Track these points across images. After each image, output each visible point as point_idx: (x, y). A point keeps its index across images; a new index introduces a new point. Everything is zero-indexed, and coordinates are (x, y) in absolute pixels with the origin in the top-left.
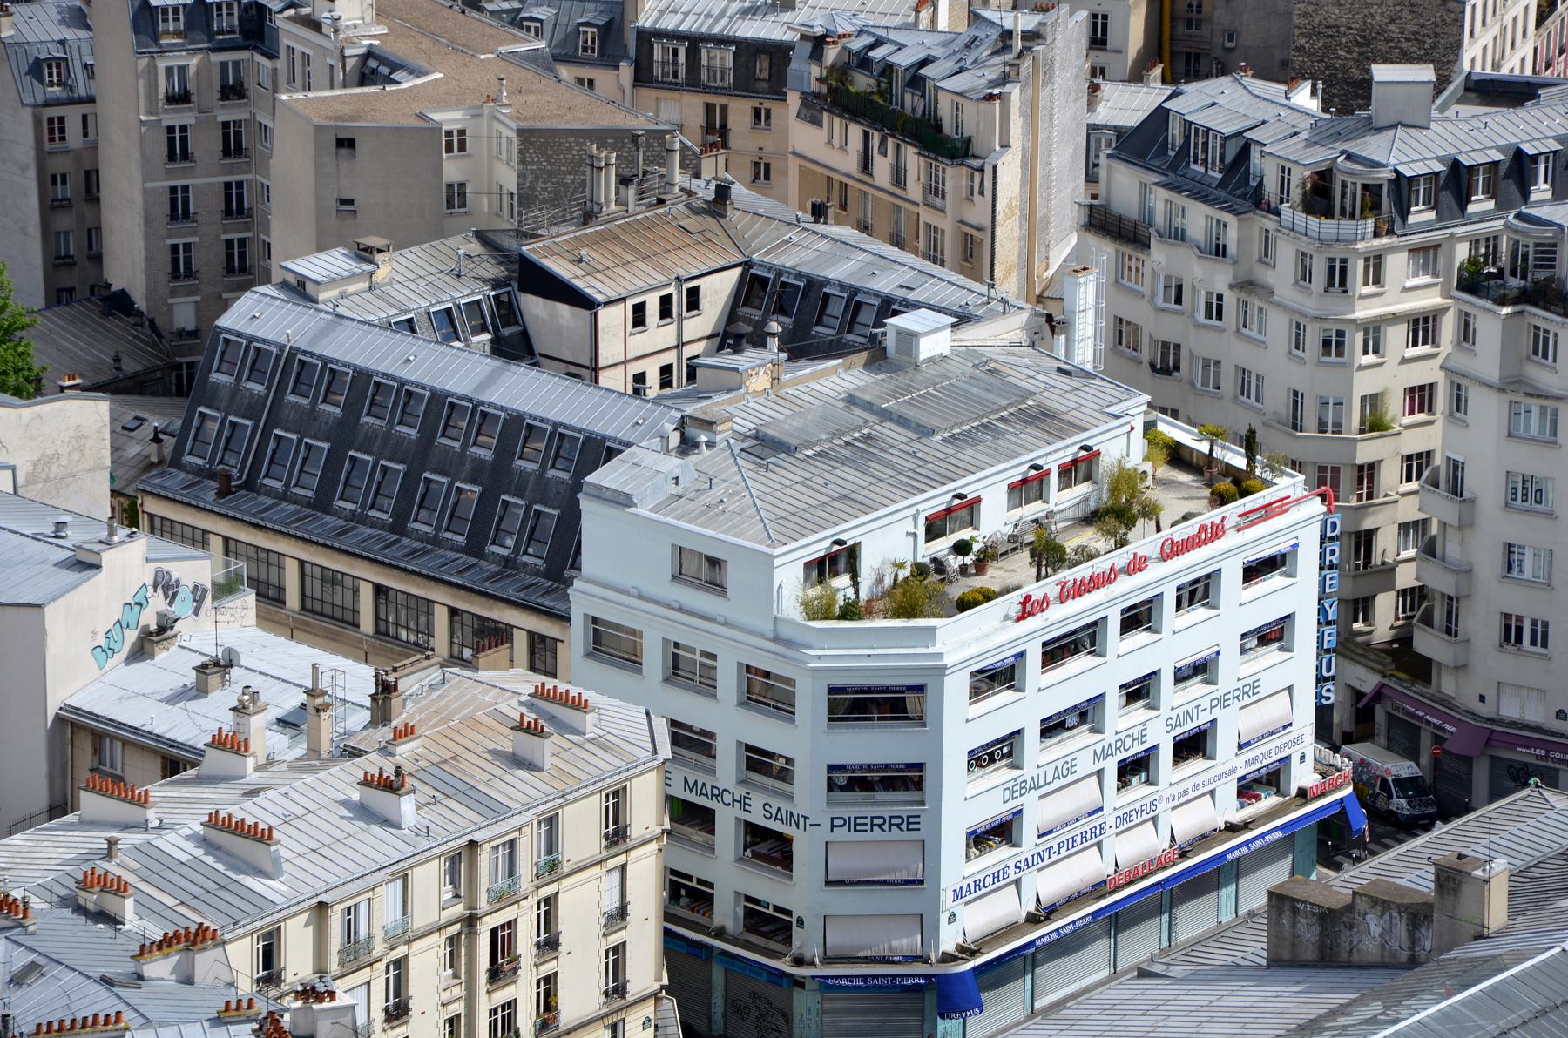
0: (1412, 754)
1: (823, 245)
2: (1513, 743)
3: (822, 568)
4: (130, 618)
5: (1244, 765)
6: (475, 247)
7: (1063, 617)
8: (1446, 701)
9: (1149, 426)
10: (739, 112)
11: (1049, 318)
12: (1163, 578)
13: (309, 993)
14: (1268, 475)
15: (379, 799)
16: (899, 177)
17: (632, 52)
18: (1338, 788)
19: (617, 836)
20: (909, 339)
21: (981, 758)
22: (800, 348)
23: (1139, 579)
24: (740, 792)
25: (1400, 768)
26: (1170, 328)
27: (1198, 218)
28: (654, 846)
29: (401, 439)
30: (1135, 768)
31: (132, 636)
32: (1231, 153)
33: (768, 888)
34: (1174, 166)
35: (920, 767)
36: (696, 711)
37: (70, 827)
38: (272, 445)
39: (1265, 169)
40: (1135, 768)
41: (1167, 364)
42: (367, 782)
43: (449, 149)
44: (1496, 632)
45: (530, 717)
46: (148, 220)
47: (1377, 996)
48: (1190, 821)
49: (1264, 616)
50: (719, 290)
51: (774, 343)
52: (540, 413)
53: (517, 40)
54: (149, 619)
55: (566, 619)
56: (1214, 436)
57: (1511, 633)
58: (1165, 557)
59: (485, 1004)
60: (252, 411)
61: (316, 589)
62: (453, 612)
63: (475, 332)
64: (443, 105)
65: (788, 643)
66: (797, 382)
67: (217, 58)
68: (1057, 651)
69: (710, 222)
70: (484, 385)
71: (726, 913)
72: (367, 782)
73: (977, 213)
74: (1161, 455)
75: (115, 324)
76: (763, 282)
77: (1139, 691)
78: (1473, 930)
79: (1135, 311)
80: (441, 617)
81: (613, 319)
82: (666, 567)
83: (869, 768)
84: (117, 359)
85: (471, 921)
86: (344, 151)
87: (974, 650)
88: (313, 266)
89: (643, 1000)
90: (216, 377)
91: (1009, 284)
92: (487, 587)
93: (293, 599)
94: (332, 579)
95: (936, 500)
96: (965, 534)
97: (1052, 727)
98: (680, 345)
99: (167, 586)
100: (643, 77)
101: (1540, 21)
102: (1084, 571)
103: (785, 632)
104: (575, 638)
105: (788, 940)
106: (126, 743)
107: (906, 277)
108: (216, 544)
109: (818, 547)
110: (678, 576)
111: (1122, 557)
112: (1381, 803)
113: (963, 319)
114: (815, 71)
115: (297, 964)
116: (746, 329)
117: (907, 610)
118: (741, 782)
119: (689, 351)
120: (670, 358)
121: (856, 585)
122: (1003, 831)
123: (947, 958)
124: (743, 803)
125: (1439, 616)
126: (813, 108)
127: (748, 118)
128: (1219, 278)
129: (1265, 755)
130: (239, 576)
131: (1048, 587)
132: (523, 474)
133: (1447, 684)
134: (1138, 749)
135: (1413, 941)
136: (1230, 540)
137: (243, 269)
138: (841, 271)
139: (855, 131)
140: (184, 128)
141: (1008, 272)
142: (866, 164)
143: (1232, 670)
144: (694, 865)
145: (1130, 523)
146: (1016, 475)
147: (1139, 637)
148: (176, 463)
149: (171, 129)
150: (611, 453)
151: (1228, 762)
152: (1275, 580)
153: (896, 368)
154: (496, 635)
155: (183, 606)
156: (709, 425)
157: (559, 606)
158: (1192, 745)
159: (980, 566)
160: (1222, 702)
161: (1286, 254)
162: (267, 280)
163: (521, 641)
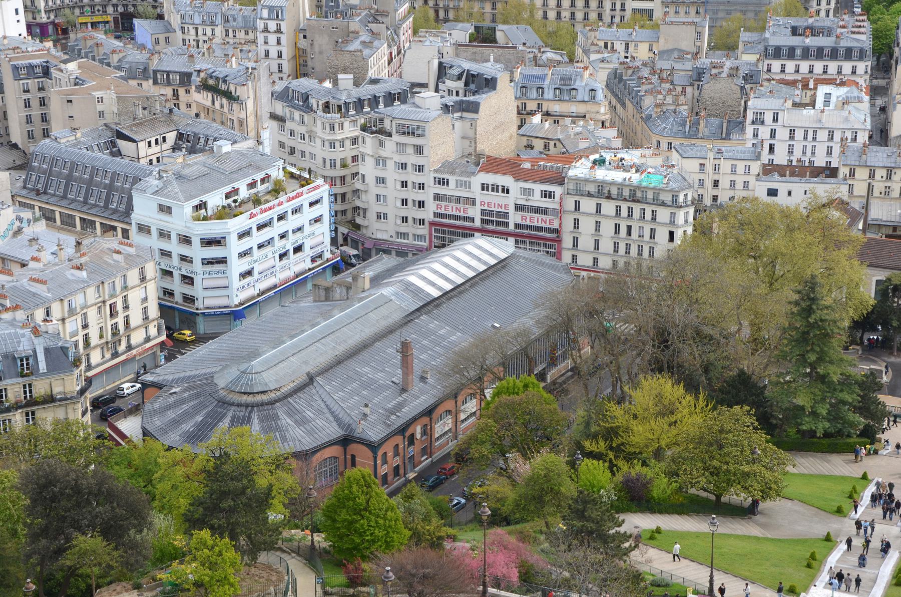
0: (357, 249)
3: (198, 207)
4: (10, 228)
5: (312, 253)
7: (262, 218)
8: (364, 235)
9: (284, 169)
10: (182, 92)
12: (288, 207)
14: (314, 179)
16: (222, 106)
17: (152, 76)
21: (242, 255)
23: (281, 207)
25: (354, 252)
27: (297, 114)
30: (282, 256)
31: (11, 233)
32: (305, 98)
33: (188, 290)
34: (290, 101)
35: (226, 258)
36: (166, 246)
39: (313, 102)
40: (282, 256)
43: (98, 102)
46: (20, 124)
48: (298, 268)
49: (316, 215)
50: (171, 137)
51: (184, 150)
53: (117, 73)
54: (15, 228)
56: (301, 169)
57: (379, 216)
58: (288, 201)
59: (110, 323)
60: (44, 173)
64: (95, 90)
66: (190, 160)
67: (36, 80)
68: (260, 227)
71: (178, 298)
73: (242, 115)
74: (288, 176)
75: (14, 152)
77: (283, 236)
78: (361, 290)
79: (283, 139)
80: (98, 225)
83: (212, 259)
85: (104, 302)
86: (69, 104)
87: (238, 227)
89: (92, 306)
90: (34, 164)
92: (110, 217)
94: (70, 216)
95: (228, 189)
96: (235, 198)
97: (260, 246)
99: (20, 220)
100: (155, 82)
101: (389, 64)
102: (267, 206)
105: (194, 304)
109: (196, 202)
111: (277, 201)
112: (349, 261)
113: (234, 143)
114: (198, 79)
117: (220, 217)
121: (206, 212)
122: (249, 273)
123: (236, 306)
126: (199, 89)
127: (185, 92)
128: (302, 130)
129: (318, 250)
131: (257, 210)
132: (117, 186)
134: (284, 251)
135: (347, 294)
136: (305, 196)
139: (210, 95)
140: (28, 99)
141: (252, 130)
142: (213, 103)
143: (307, 229)
145: (278, 193)
147: (282, 222)
149: (25, 100)
151: (308, 252)
152: (318, 206)
155: (25, 224)
157: (129, 222)
158: (298, 249)
159: (240, 205)
160: (305, 238)
161: (319, 123)
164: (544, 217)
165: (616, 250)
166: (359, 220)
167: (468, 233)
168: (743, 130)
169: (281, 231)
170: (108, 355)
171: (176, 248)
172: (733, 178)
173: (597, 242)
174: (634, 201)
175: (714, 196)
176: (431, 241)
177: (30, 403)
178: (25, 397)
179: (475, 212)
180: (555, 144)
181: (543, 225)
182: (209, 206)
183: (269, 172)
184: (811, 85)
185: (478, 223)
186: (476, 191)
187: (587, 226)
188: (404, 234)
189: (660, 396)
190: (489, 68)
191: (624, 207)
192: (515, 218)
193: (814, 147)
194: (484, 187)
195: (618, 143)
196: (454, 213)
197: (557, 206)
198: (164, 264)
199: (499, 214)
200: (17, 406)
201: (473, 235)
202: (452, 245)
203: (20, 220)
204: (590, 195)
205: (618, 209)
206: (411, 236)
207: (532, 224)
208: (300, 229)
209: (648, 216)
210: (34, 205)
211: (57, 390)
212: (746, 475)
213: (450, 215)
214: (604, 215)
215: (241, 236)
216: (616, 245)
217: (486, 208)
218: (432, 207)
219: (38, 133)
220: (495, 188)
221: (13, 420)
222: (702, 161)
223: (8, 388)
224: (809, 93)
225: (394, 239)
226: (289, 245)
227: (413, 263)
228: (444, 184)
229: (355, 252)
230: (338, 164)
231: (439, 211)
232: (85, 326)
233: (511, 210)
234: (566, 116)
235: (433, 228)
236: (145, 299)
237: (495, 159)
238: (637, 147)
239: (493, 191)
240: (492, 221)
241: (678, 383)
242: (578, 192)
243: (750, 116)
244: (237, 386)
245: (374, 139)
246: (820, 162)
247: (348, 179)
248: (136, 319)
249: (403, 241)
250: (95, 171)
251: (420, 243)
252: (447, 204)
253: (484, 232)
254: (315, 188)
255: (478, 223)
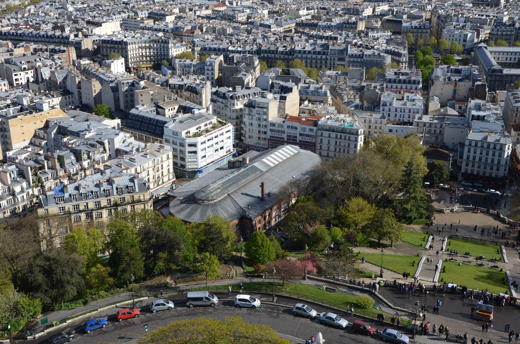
3: (187, 133)
7: (209, 137)
12: (219, 133)
16: (194, 96)
21: (202, 150)
33: (183, 163)
50: (177, 107)
94: (141, 135)
95: (197, 126)
99: (125, 137)
109: (186, 131)
122: (205, 156)
151: (225, 149)
158: (222, 148)
168: (379, 108)
170: (156, 185)
172: (376, 125)
173: (329, 147)
174: (342, 133)
177: (133, 202)
179: (285, 136)
182: (191, 132)
183: (212, 120)
184: (402, 93)
185: (286, 139)
187: (325, 141)
189: (358, 205)
190: (290, 84)
192: (299, 138)
193: (404, 115)
194: (288, 127)
195: (336, 112)
199: (293, 137)
200: (129, 203)
208: (222, 141)
211: (142, 198)
212: (390, 233)
215: (202, 143)
216: (336, 148)
218: (269, 134)
224: (401, 96)
226: (218, 147)
227: (264, 154)
229: (241, 149)
232: (148, 175)
236: (169, 166)
237: (292, 117)
238: (342, 113)
241: (365, 200)
243: (381, 103)
246: (406, 120)
248: (165, 173)
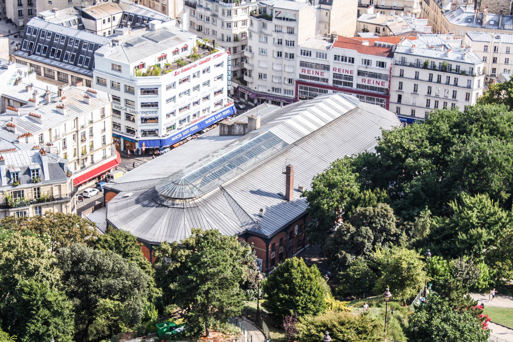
1: (137, 8)
2: (261, 96)
6: (73, 9)
7: (183, 76)
8: (249, 89)
9: (197, 40)
11: (179, 21)
13: (49, 145)
15: (60, 110)
18: (231, 104)
19: (103, 116)
20: (153, 25)
22: (134, 27)
24: (125, 108)
26: (200, 23)
28: (110, 118)
29: (61, 45)
31: (14, 81)
35: (157, 103)
36: (117, 93)
37: (4, 115)
38: (38, 46)
41: (200, 29)
42: (57, 107)
44: (258, 76)
45: (86, 95)
46: (14, 6)
47: (238, 140)
49: (219, 74)
50: (118, 17)
51: (129, 26)
52: (72, 36)
55: (92, 77)
61: (47, 72)
62: (72, 76)
63: (74, 25)
65: (133, 81)
69: (116, 4)
70: (76, 35)
72: (57, 107)
75: (9, 24)
76: (127, 15)
77: (197, 88)
79: (194, 20)
80: (70, 77)
81: (99, 22)
82: (111, 67)
84: (9, 31)
88: (43, 13)
91: (171, 15)
93: (56, 78)
94: (50, 71)
95: (159, 55)
98: (112, 27)
99: (20, 73)
103: (132, 79)
104: (94, 81)
106: (14, 100)
107: (152, 14)
108: (28, 64)
109: (138, 63)
110: (113, 69)
113: (163, 21)
115: (46, 140)
116: (123, 24)
118: (126, 106)
119: (113, 28)
120: (110, 29)
123: (163, 136)
124: (126, 110)
125: (248, 74)
128: (208, 14)
130: (33, 70)
132: (84, 51)
133: (250, 86)
137: (31, 14)
138: (140, 13)
144: (117, 121)
146: (174, 50)
148: (20, 50)
150: (100, 47)
153: (152, 30)
154: (80, 80)
156: (117, 41)
162: (36, 16)
163: (84, 81)
164: (378, 80)
165: (428, 106)
166: (246, 78)
167: (324, 89)
169: (195, 85)
171: (122, 95)
174: (442, 71)
175: (493, 69)
176: (296, 94)
178: (35, 197)
179: (329, 75)
180: (384, 29)
181: (377, 86)
185: (330, 83)
186: (330, 61)
188: (278, 89)
191: (435, 74)
192: (357, 80)
194: (336, 58)
196: (314, 75)
197: (388, 73)
198: (115, 106)
199: (346, 77)
201: (326, 92)
202: (315, 98)
203: (20, 73)
204: (411, 65)
205: (431, 76)
206: (283, 91)
207: (369, 85)
209: (452, 82)
210: (26, 62)
211: (56, 193)
213: (311, 77)
214: (421, 80)
215: (168, 88)
217: (337, 72)
219: (25, 13)
220: (344, 59)
221: (27, 211)
222: (486, 44)
223: (25, 190)
225: (271, 92)
228: (307, 55)
230: (232, 39)
231: (303, 74)
233: (355, 74)
234: (391, 9)
235: (299, 85)
239: (342, 60)
240: (341, 82)
242: (403, 63)
244: (172, 194)
245: (260, 22)
247: (239, 49)
248: (98, 144)
249: (277, 94)
250: (68, 39)
251: (289, 96)
252: (309, 69)
253: (335, 89)
254: (218, 55)
255: (330, 83)
